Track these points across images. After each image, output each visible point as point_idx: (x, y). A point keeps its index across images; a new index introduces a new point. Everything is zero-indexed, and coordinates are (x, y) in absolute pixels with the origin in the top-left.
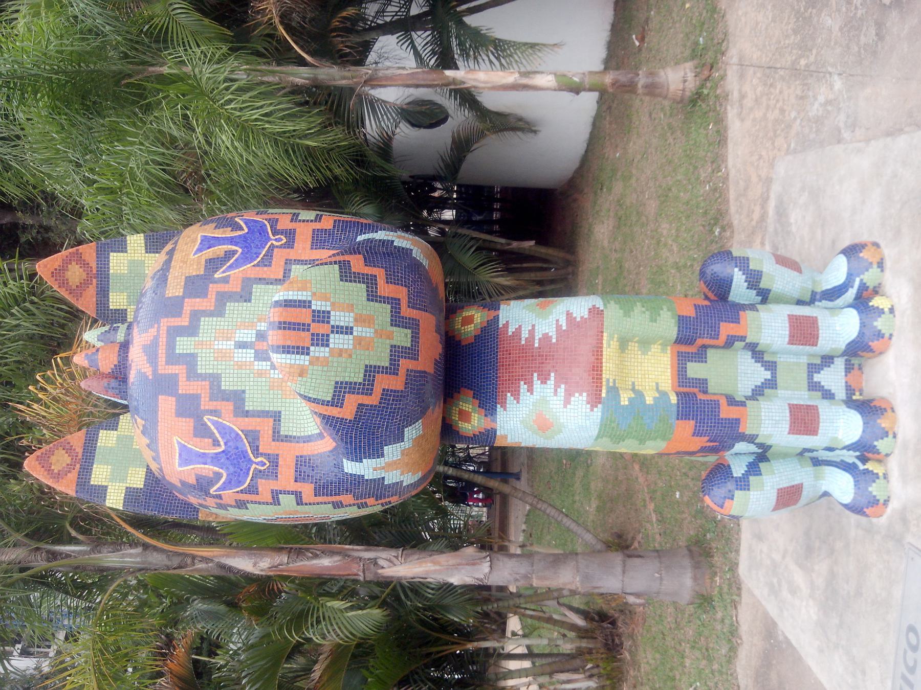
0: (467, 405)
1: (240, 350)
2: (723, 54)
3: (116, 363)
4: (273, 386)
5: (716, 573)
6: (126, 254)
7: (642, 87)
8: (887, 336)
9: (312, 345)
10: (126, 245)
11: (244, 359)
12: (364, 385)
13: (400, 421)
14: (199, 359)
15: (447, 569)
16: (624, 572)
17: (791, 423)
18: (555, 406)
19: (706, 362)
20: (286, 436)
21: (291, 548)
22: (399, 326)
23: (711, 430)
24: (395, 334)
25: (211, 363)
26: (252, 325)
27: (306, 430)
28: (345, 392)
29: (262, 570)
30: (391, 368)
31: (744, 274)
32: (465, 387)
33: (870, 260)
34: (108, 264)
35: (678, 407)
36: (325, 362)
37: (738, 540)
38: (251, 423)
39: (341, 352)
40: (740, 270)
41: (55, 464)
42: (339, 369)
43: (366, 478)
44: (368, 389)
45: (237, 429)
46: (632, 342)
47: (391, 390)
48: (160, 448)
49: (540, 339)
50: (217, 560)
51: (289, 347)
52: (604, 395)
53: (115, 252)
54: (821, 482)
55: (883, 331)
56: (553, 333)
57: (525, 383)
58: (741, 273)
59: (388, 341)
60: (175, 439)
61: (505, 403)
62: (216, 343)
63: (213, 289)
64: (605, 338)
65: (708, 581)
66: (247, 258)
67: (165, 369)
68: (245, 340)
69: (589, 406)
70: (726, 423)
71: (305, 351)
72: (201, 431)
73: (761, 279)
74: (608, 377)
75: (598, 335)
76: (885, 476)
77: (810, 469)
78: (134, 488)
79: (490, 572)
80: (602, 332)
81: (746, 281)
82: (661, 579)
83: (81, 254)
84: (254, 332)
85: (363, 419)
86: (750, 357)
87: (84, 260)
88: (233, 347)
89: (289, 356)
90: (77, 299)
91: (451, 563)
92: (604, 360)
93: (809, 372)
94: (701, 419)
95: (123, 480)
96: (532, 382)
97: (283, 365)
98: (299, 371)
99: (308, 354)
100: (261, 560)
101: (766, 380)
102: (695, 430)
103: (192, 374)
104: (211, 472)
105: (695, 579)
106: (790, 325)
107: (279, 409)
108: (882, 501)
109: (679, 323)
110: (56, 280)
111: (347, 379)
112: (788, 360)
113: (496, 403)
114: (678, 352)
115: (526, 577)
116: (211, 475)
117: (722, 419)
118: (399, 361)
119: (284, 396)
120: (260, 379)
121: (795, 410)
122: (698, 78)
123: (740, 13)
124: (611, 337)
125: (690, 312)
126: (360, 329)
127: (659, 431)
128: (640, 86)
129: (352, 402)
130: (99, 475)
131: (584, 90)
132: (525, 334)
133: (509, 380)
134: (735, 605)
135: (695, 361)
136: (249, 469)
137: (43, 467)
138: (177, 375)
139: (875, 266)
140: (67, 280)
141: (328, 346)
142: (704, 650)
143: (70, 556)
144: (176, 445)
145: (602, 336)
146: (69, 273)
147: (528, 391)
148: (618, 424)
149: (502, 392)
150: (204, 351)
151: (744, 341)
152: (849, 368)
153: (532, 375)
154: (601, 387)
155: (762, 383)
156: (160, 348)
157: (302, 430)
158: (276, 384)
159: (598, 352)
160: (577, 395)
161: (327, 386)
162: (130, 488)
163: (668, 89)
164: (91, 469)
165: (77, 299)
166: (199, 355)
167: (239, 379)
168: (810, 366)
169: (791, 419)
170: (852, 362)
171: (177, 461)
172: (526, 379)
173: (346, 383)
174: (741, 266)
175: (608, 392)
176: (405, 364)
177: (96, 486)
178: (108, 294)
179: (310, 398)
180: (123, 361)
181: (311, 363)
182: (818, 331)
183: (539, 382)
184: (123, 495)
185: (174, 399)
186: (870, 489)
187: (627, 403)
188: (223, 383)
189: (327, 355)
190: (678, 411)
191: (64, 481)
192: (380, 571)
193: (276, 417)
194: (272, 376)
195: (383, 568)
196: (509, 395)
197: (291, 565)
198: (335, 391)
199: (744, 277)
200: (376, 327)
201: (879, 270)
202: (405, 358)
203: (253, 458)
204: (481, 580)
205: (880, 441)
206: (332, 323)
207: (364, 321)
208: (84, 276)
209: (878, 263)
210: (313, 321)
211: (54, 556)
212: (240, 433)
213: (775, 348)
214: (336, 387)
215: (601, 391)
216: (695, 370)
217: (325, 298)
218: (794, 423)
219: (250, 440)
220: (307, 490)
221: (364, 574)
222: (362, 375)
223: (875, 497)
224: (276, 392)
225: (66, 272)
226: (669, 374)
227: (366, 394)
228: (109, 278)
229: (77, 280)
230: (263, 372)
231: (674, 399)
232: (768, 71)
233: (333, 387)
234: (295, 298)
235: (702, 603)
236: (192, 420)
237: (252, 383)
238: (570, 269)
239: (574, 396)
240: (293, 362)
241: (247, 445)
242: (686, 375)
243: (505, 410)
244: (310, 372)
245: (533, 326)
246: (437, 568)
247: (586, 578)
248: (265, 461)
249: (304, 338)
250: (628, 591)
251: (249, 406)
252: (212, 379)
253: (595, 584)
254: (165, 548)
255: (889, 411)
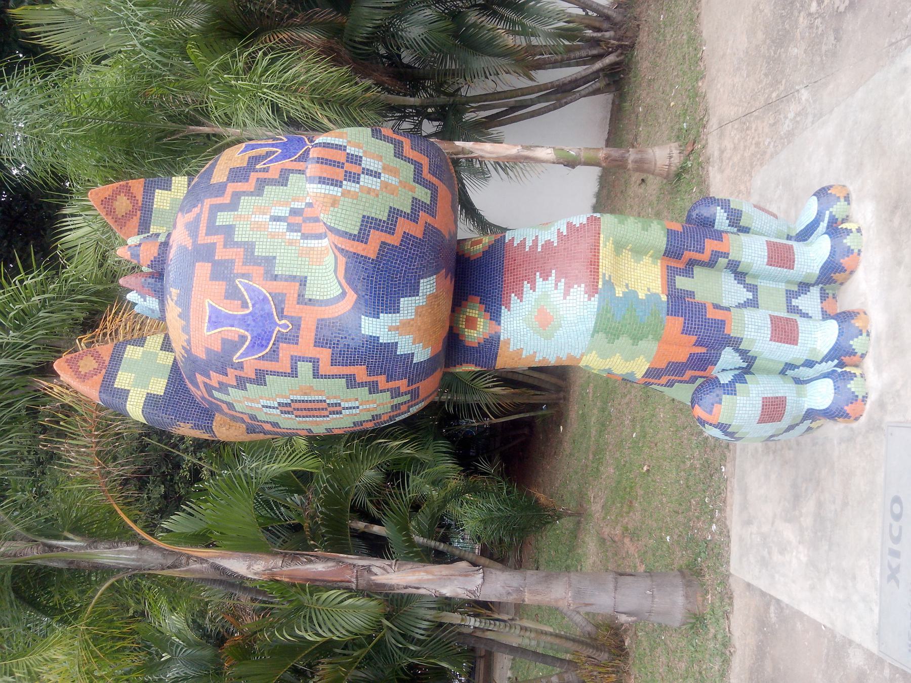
0: (474, 311)
1: (274, 223)
2: (704, 127)
3: (156, 255)
4: (302, 253)
5: (707, 592)
6: (169, 192)
7: (632, 162)
8: (856, 251)
9: (345, 180)
10: (171, 184)
11: (277, 230)
12: (388, 224)
13: (417, 269)
14: (237, 229)
15: (440, 579)
16: (616, 590)
17: (772, 330)
18: (555, 299)
19: (693, 277)
20: (310, 300)
21: (286, 554)
22: (421, 184)
23: (698, 328)
24: (417, 189)
25: (247, 232)
26: (286, 204)
27: (329, 293)
28: (370, 227)
29: (255, 574)
30: (411, 216)
31: (725, 212)
32: (473, 294)
33: (837, 195)
34: (153, 199)
35: (668, 304)
36: (355, 196)
37: (728, 552)
38: (278, 287)
39: (369, 191)
40: (722, 208)
41: (82, 367)
42: (367, 205)
43: (381, 341)
44: (391, 229)
45: (265, 292)
46: (626, 249)
47: (411, 236)
48: (191, 314)
49: (542, 246)
50: (212, 561)
51: (324, 178)
52: (600, 286)
53: (160, 189)
54: (803, 399)
55: (852, 248)
56: (555, 239)
57: (528, 283)
58: (723, 211)
59: (410, 193)
60: (207, 301)
61: (510, 303)
62: (253, 216)
63: (254, 176)
64: (601, 239)
65: (700, 598)
66: (284, 156)
67: (203, 239)
68: (280, 215)
69: (586, 296)
70: (712, 323)
71: (337, 183)
72: (233, 294)
73: (741, 217)
74: (604, 272)
75: (595, 236)
76: (862, 376)
77: (793, 386)
78: (154, 395)
79: (483, 584)
80: (599, 234)
81: (727, 219)
82: (653, 596)
83: (130, 187)
84: (288, 209)
85: (385, 260)
86: (733, 279)
87: (132, 193)
88: (268, 220)
89: (324, 186)
90: (121, 228)
91: (444, 573)
92: (601, 257)
93: (787, 297)
94: (689, 317)
95: (145, 386)
96: (535, 280)
97: (318, 195)
98: (331, 201)
99: (341, 187)
100: (255, 562)
101: (748, 299)
102: (684, 327)
103: (229, 242)
104: (237, 336)
105: (687, 597)
106: (768, 249)
107: (306, 274)
108: (860, 397)
109: (668, 235)
110: (105, 208)
111: (373, 215)
112: (768, 285)
113: (500, 305)
114: (668, 266)
115: (519, 591)
116: (237, 339)
117: (709, 319)
118: (419, 212)
119: (311, 263)
120: (290, 247)
121: (775, 320)
122: (682, 155)
123: (719, 86)
124: (607, 239)
125: (677, 227)
126: (387, 176)
127: (651, 325)
128: (630, 161)
129: (376, 237)
130: (123, 380)
131: (580, 163)
132: (529, 243)
133: (514, 282)
134: (727, 616)
135: (683, 276)
136: (273, 330)
137: (71, 368)
138: (215, 244)
139: (842, 200)
140: (114, 209)
141: (358, 183)
142: (697, 675)
143: (67, 549)
144: (207, 308)
145: (599, 237)
146: (117, 203)
147: (531, 289)
148: (613, 315)
149: (507, 293)
150: (242, 222)
151: (727, 258)
152: (824, 297)
153: (535, 274)
154: (598, 279)
155: (745, 302)
156: (202, 222)
157: (325, 293)
158: (304, 252)
159: (595, 249)
160: (576, 286)
161: (355, 219)
162: (151, 394)
163: (655, 164)
164: (116, 375)
165: (121, 228)
166: (237, 226)
167: (272, 247)
168: (788, 292)
169: (772, 326)
170: (827, 291)
171: (206, 324)
172: (529, 279)
173: (372, 218)
174: (722, 206)
175: (604, 284)
176: (423, 216)
177: (119, 389)
178: (149, 226)
179: (338, 231)
180: (163, 253)
181: (343, 194)
182: (794, 255)
183: (541, 279)
184: (144, 399)
185: (210, 264)
186: (849, 386)
187: (621, 295)
188: (256, 250)
189: (357, 190)
190: (668, 307)
191: (90, 382)
192: (373, 578)
193: (303, 282)
194: (301, 245)
195: (376, 575)
196: (513, 295)
197: (285, 568)
198: (362, 225)
199: (726, 214)
200: (401, 179)
201: (846, 203)
202: (425, 211)
203: (277, 320)
204: (473, 593)
205: (856, 340)
206: (363, 166)
207: (391, 171)
208: (130, 206)
209: (845, 197)
210: (347, 161)
211: (51, 548)
212: (268, 295)
213: (754, 269)
214: (363, 221)
215: (598, 282)
216: (682, 283)
217: (358, 146)
218: (776, 330)
219: (277, 302)
220: (325, 355)
221: (357, 580)
222: (386, 214)
223: (853, 393)
224: (304, 259)
225: (114, 202)
226: (660, 283)
227: (389, 233)
228: (152, 212)
229: (123, 210)
230: (294, 241)
231: (664, 298)
232: (743, 119)
233: (360, 221)
234: (333, 142)
235: (695, 624)
236: (224, 283)
237: (282, 251)
238: (562, 395)
239: (573, 287)
240: (327, 192)
241: (273, 307)
242: (675, 286)
243: (509, 310)
244: (341, 203)
245: (537, 237)
246: (430, 577)
247: (578, 593)
248: (288, 323)
249: (339, 174)
250: (620, 609)
251: (278, 271)
252: (246, 247)
253: (587, 601)
254: (162, 546)
255: (862, 315)
